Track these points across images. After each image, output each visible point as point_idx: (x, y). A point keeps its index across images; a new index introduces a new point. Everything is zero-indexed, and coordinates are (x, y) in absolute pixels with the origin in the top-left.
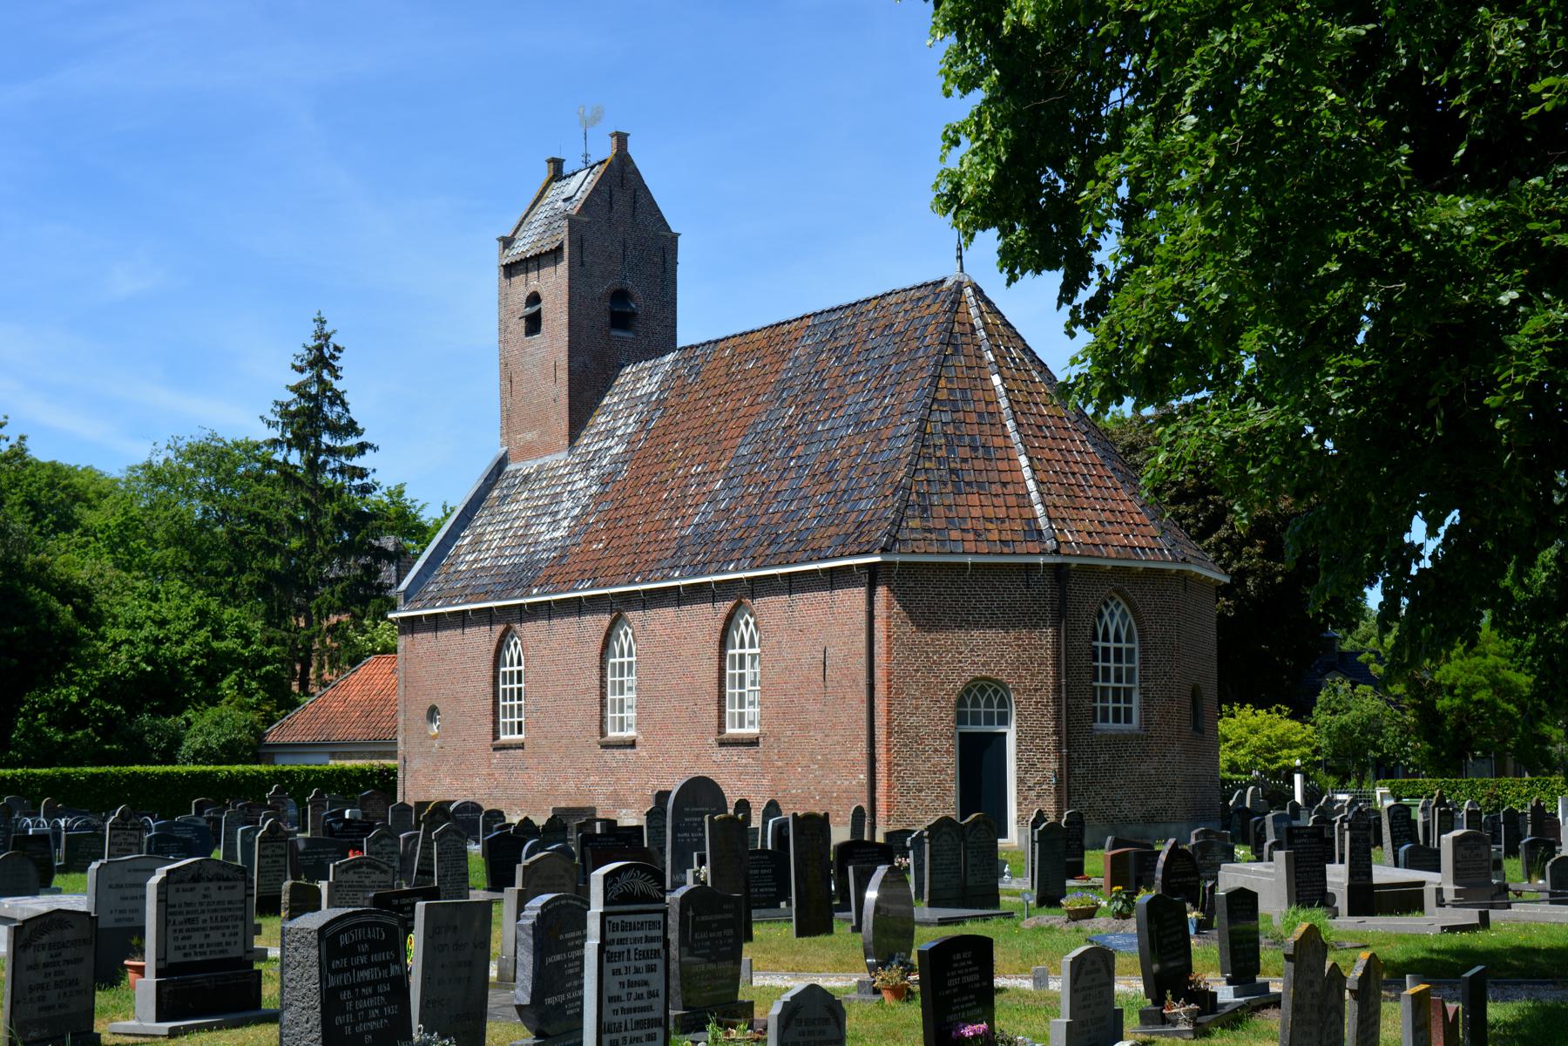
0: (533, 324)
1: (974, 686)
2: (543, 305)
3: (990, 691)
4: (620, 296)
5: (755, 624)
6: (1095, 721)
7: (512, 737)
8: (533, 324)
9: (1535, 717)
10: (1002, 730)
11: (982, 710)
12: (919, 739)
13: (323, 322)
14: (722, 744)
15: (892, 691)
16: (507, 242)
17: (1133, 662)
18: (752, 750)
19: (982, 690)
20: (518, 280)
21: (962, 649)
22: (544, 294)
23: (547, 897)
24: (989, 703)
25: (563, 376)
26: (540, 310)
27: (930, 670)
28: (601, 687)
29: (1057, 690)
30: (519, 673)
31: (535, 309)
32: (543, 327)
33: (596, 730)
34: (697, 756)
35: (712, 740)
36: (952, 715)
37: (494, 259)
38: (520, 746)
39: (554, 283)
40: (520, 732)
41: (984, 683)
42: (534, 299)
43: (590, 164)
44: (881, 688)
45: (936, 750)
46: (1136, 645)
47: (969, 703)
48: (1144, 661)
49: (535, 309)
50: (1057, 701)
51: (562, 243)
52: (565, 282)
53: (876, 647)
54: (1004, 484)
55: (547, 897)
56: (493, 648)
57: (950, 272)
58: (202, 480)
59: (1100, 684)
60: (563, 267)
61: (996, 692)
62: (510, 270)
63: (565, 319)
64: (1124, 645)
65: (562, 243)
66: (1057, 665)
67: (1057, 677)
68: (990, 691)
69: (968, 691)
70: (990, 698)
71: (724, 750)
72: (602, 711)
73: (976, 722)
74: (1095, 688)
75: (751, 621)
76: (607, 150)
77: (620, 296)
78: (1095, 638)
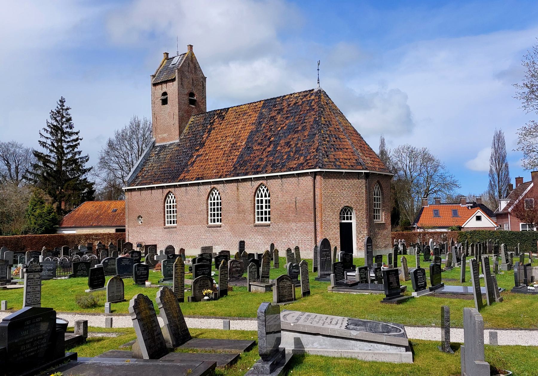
0: (165, 102)
1: (343, 209)
2: (168, 96)
3: (347, 210)
4: (192, 94)
5: (175, 197)
6: (375, 219)
8: (165, 102)
11: (349, 216)
13: (167, 54)
14: (256, 226)
16: (154, 76)
17: (257, 206)
19: (345, 210)
21: (341, 197)
22: (168, 92)
24: (347, 214)
25: (177, 117)
26: (167, 98)
28: (207, 210)
30: (220, 202)
31: (165, 97)
33: (205, 222)
37: (150, 81)
38: (176, 227)
39: (172, 89)
40: (221, 222)
41: (346, 208)
42: (165, 94)
43: (180, 54)
44: (318, 209)
45: (334, 228)
46: (381, 197)
47: (349, 213)
48: (383, 202)
49: (165, 97)
51: (175, 77)
53: (316, 197)
54: (347, 149)
56: (164, 198)
57: (316, 87)
59: (376, 208)
61: (349, 210)
62: (155, 85)
65: (175, 77)
68: (347, 210)
69: (342, 210)
70: (344, 212)
72: (207, 217)
73: (344, 219)
74: (374, 209)
75: (173, 196)
76: (186, 50)
77: (192, 94)
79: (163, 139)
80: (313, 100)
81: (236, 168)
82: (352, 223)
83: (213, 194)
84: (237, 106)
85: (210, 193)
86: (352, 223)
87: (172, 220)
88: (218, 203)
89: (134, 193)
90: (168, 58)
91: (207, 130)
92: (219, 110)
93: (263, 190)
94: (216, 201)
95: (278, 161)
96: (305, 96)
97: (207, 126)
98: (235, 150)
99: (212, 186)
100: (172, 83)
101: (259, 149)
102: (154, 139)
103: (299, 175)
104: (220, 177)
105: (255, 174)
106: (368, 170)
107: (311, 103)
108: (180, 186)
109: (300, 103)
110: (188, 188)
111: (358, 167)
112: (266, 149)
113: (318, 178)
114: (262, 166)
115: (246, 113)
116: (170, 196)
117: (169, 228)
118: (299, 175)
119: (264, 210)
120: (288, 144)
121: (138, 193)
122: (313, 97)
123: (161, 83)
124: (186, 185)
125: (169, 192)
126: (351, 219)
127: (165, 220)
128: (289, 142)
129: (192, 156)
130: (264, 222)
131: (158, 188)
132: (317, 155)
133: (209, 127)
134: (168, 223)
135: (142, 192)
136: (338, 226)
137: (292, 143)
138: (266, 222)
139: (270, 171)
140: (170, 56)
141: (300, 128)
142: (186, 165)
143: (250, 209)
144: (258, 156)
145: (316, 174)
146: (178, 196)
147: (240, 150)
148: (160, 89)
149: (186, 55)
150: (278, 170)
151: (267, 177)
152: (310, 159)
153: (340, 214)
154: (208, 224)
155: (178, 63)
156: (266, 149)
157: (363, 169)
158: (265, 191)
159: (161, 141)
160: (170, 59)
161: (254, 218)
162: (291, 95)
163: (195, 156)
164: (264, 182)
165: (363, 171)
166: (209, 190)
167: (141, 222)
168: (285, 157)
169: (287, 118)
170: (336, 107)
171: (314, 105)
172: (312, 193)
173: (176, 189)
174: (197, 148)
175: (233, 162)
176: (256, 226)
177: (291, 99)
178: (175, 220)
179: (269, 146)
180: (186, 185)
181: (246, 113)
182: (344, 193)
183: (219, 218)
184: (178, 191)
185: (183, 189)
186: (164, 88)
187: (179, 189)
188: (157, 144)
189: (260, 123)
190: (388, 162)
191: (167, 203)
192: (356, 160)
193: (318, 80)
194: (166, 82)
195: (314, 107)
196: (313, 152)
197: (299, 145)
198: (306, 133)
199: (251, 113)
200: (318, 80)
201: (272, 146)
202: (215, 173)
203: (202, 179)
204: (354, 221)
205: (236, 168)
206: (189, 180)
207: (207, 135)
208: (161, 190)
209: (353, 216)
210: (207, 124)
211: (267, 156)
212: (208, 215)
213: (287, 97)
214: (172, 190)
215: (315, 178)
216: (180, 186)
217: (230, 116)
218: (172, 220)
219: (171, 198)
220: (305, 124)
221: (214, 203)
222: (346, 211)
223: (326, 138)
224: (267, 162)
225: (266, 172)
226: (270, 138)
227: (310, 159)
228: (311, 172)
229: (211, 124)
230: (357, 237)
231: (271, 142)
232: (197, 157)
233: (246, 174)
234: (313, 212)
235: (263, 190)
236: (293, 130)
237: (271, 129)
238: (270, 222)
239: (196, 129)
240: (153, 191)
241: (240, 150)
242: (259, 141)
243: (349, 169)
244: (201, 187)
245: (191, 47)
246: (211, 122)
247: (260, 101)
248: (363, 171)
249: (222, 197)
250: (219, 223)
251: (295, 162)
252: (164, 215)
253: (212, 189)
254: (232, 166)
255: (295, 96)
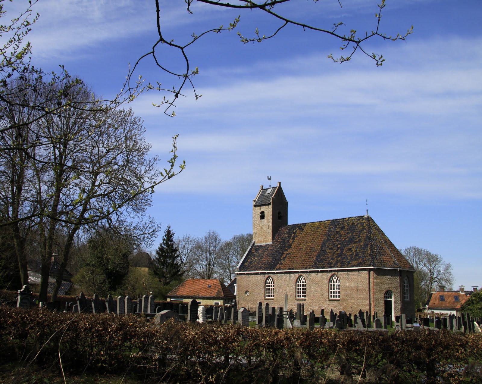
4: (279, 213)
7: (334, 298)
9: (92, 301)
10: (390, 299)
12: (379, 301)
13: (263, 186)
14: (330, 300)
15: (374, 292)
18: (338, 302)
19: (388, 292)
20: (258, 208)
23: (71, 303)
27: (380, 288)
29: (400, 292)
32: (265, 218)
34: (323, 303)
35: (327, 300)
36: (384, 297)
38: (273, 299)
50: (400, 294)
52: (271, 210)
55: (71, 303)
58: (11, 338)
60: (271, 206)
63: (271, 217)
64: (268, 291)
66: (400, 288)
67: (400, 290)
71: (330, 302)
76: (278, 185)
78: (273, 292)
79: (261, 242)
80: (364, 222)
81: (316, 263)
82: (391, 300)
83: (300, 279)
84: (312, 223)
85: (298, 278)
86: (391, 300)
87: (270, 294)
88: (303, 285)
89: (243, 276)
90: (264, 190)
91: (292, 237)
92: (299, 224)
93: (302, 279)
94: (302, 284)
95: (344, 260)
96: (359, 220)
97: (291, 235)
98: (314, 251)
99: (300, 274)
100: (268, 206)
101: (330, 252)
102: (253, 241)
103: (359, 270)
104: (306, 269)
105: (330, 268)
106: (401, 268)
107: (363, 224)
108: (277, 273)
109: (356, 224)
110: (283, 275)
111: (395, 266)
112: (335, 252)
113: (372, 272)
114: (334, 263)
115: (319, 228)
116: (269, 279)
117: (268, 299)
118: (359, 270)
119: (335, 290)
120: (350, 250)
121: (246, 276)
122: (364, 221)
123: (260, 206)
124: (281, 273)
125: (269, 277)
126: (391, 298)
127: (265, 295)
128: (351, 249)
129: (283, 254)
130: (335, 298)
131: (261, 273)
132: (370, 258)
133: (293, 235)
134: (267, 296)
135: (249, 276)
136: (383, 302)
137: (352, 249)
138: (336, 298)
139: (340, 266)
140: (264, 188)
141: (357, 240)
142: (280, 260)
143: (327, 290)
144: (330, 256)
145: (370, 269)
146: (341, 278)
147: (317, 252)
148: (259, 210)
149: (277, 188)
150: (345, 266)
151: (347, 270)
152: (365, 260)
153: (385, 295)
154: (296, 298)
155: (271, 193)
156: (335, 252)
157: (398, 268)
158: (303, 279)
159: (258, 243)
160: (265, 189)
161: (329, 296)
162: (349, 218)
163: (285, 254)
164: (336, 273)
165: (398, 269)
166: (297, 277)
167: (248, 295)
168: (349, 258)
169: (348, 233)
170: (378, 227)
171: (365, 226)
172: (367, 282)
173: (274, 275)
174: (286, 249)
175: (313, 259)
176: (330, 300)
177: (350, 221)
178: (272, 294)
179: (337, 250)
180: (281, 273)
181: (319, 228)
182: (387, 282)
183: (304, 294)
184: (275, 276)
185: (279, 275)
186: (263, 209)
187: (276, 275)
188: (255, 245)
189: (329, 235)
190: (73, 217)
191: (267, 283)
192: (393, 262)
193: (367, 210)
194: (264, 205)
195: (365, 227)
196: (368, 256)
197: (358, 251)
198: (362, 244)
199: (322, 228)
200: (367, 210)
201: (339, 250)
202: (301, 266)
203: (293, 269)
204: (393, 299)
205: (316, 263)
206: (283, 269)
207: (292, 240)
208: (263, 275)
209: (393, 297)
210: (291, 233)
211: (336, 257)
212: (296, 292)
213: (347, 219)
214: (271, 275)
215: (369, 272)
216: (277, 273)
217: (307, 230)
218: (270, 294)
219: (270, 280)
220: (360, 238)
221: (300, 285)
222: (388, 294)
223: (375, 247)
224: (337, 260)
225: (337, 267)
226: (337, 246)
227: (365, 260)
228: (367, 269)
229: (295, 233)
230: (395, 309)
231: (338, 248)
232: (286, 255)
233: (324, 268)
234: (368, 292)
235: (302, 279)
236: (351, 240)
237: (338, 239)
238: (339, 298)
239: (284, 236)
240: (257, 275)
241: (317, 252)
242: (330, 246)
243: (390, 267)
244: (292, 275)
245: (280, 183)
246: (294, 231)
247: (328, 221)
248: (398, 269)
249: (306, 281)
250: (304, 298)
251: (356, 262)
252: (265, 291)
253: (300, 276)
254: (312, 262)
255: (352, 219)
